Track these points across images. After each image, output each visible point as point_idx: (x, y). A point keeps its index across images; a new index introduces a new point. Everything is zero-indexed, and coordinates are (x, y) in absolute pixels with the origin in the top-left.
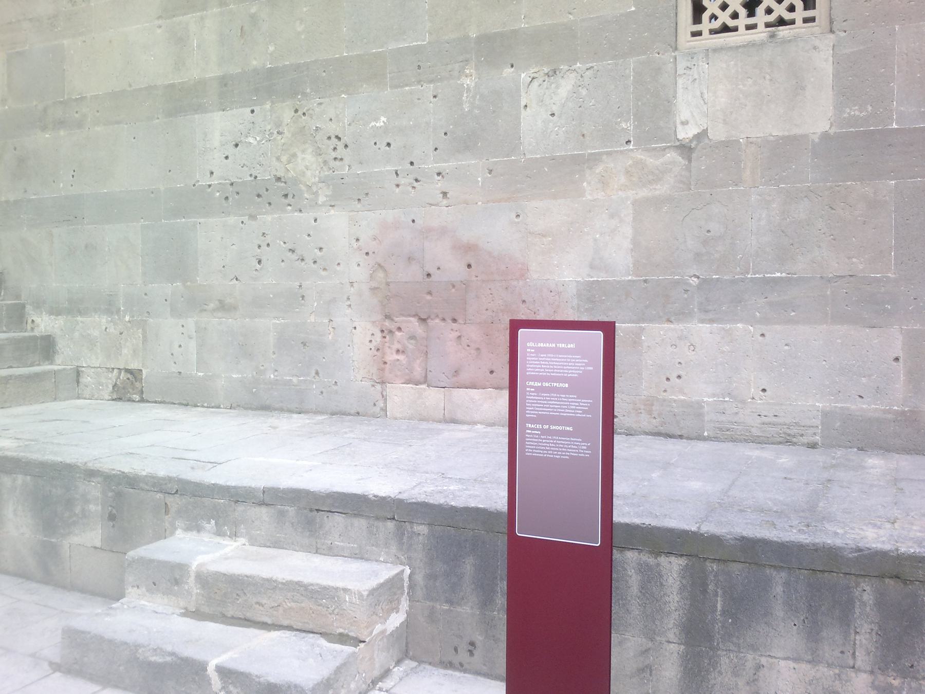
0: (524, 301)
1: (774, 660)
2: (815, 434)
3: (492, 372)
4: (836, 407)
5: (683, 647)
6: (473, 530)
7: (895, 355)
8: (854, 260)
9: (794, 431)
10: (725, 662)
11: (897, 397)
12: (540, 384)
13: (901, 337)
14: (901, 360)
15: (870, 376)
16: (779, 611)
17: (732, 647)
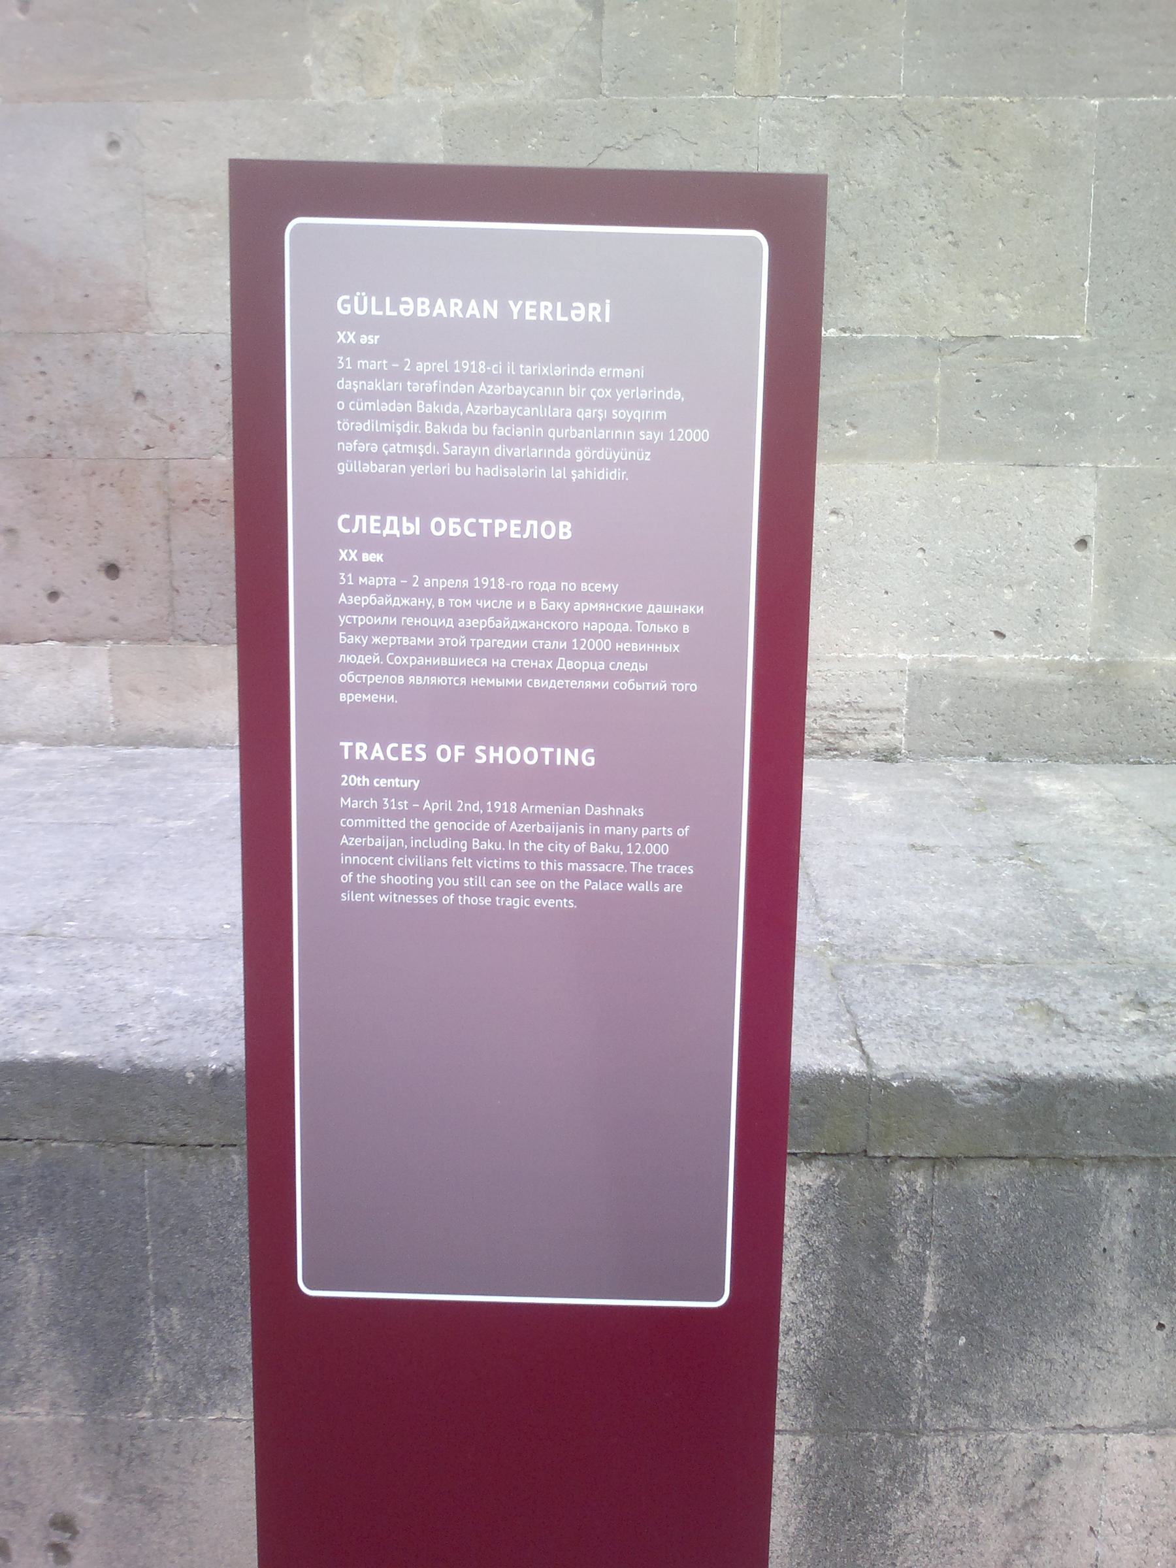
0: (139, 395)
1: (1091, 1438)
2: (893, 727)
3: (54, 595)
4: (942, 661)
5: (807, 1440)
6: (41, 1141)
7: (1079, 534)
8: (999, 297)
9: (847, 721)
10: (938, 1467)
11: (1082, 631)
12: (412, 528)
13: (1094, 488)
14: (1092, 544)
15: (1022, 583)
16: (1115, 1291)
17: (965, 1419)
